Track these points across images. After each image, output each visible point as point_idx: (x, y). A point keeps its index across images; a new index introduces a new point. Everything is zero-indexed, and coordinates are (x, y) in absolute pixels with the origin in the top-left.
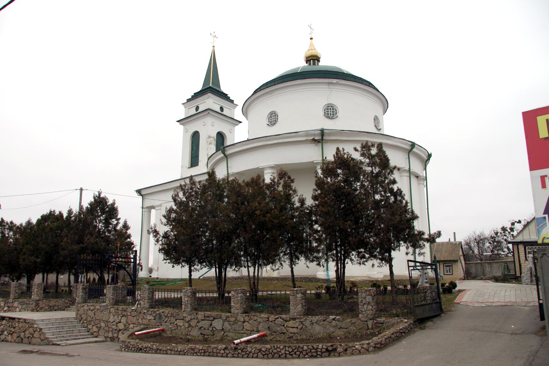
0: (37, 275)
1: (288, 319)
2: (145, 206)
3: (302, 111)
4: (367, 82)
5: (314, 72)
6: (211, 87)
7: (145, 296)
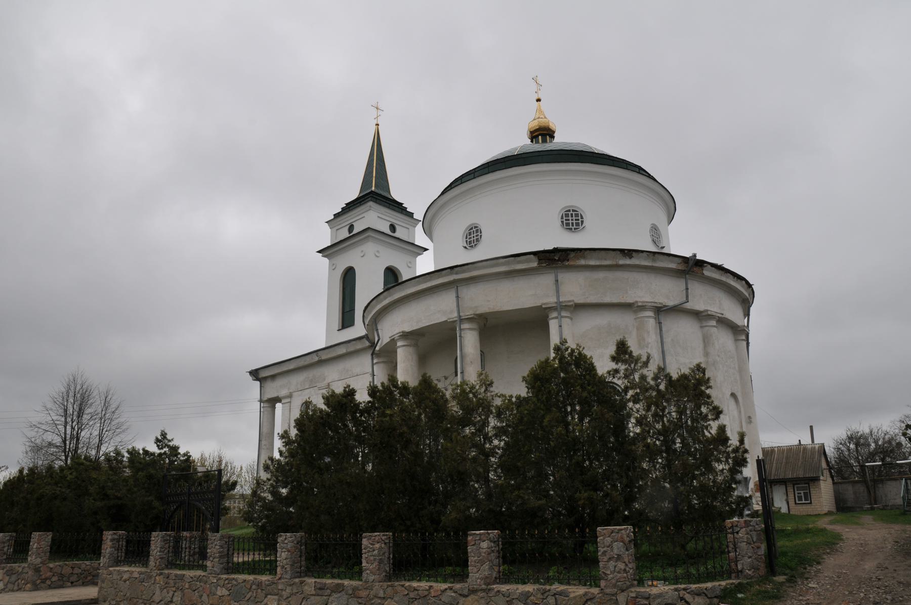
1: (466, 592)
3: (524, 220)
4: (636, 166)
5: (543, 152)
6: (375, 192)
7: (215, 551)
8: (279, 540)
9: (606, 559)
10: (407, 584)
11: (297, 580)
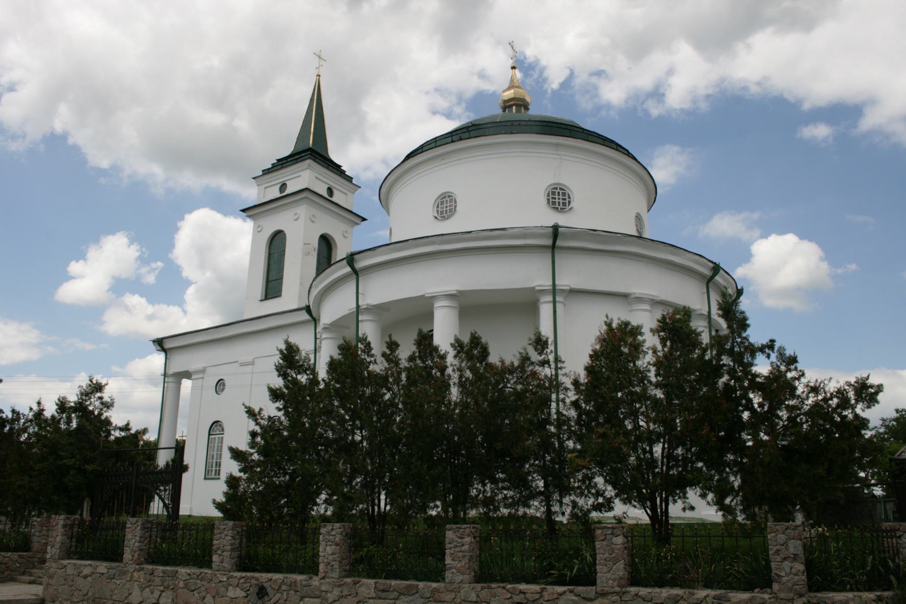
0: (790, 239)
2: (171, 371)
6: (312, 149)
7: (225, 542)
8: (323, 531)
9: (779, 558)
10: (509, 586)
11: (348, 580)
